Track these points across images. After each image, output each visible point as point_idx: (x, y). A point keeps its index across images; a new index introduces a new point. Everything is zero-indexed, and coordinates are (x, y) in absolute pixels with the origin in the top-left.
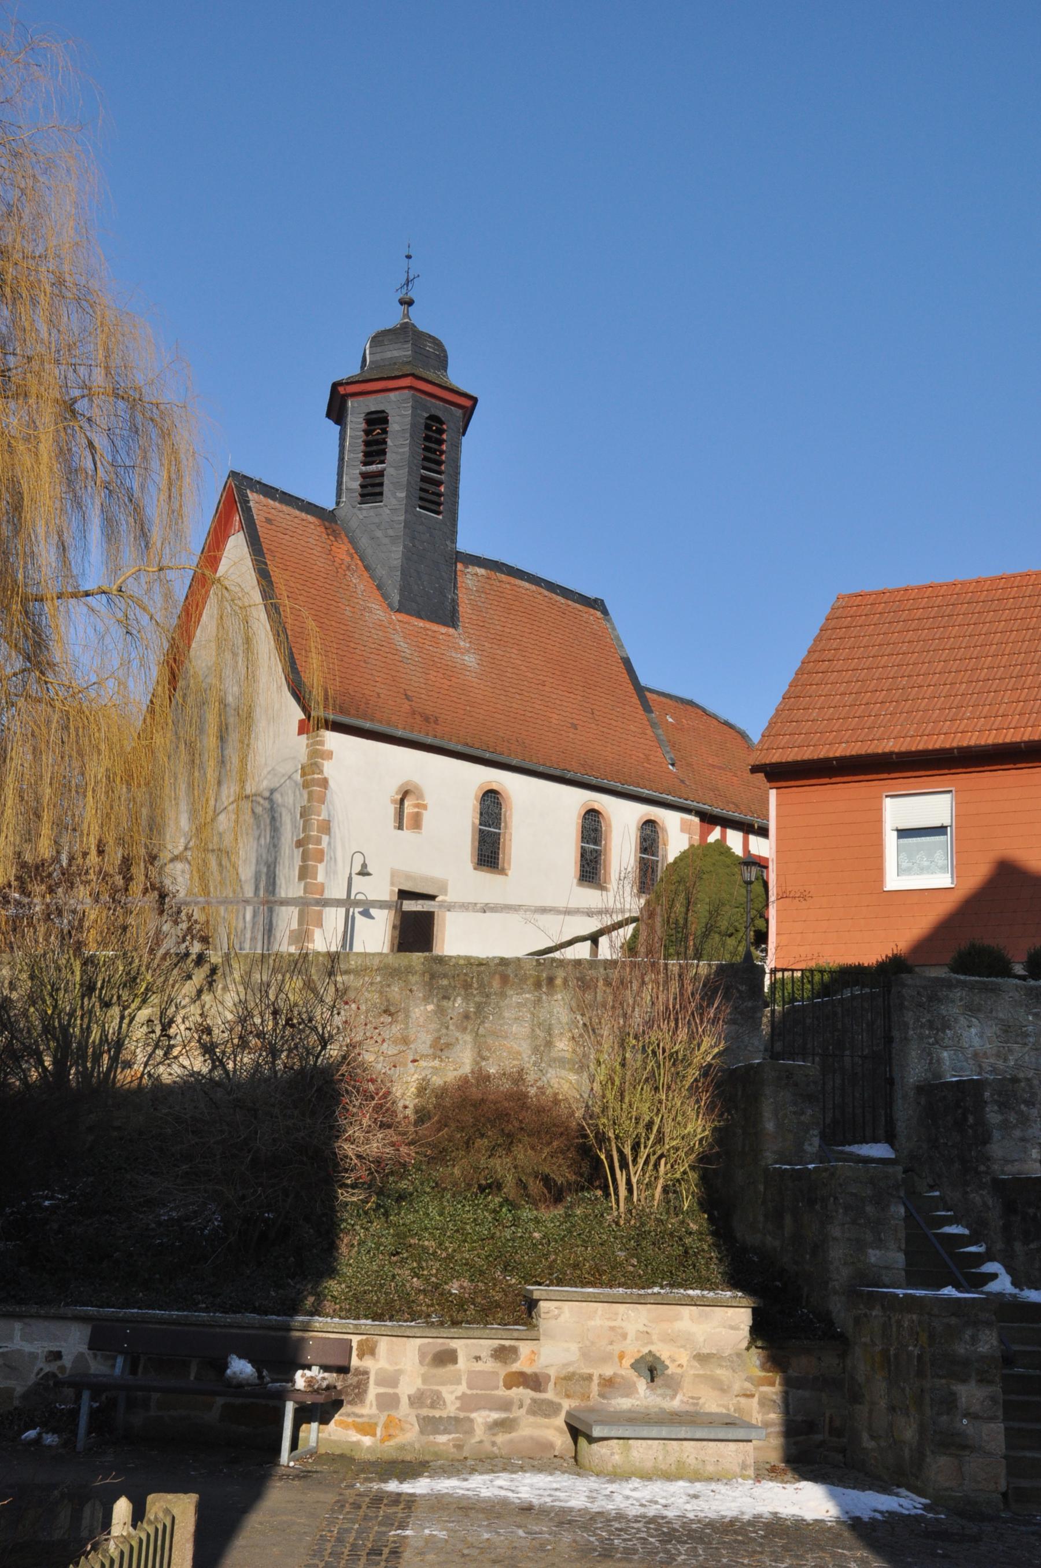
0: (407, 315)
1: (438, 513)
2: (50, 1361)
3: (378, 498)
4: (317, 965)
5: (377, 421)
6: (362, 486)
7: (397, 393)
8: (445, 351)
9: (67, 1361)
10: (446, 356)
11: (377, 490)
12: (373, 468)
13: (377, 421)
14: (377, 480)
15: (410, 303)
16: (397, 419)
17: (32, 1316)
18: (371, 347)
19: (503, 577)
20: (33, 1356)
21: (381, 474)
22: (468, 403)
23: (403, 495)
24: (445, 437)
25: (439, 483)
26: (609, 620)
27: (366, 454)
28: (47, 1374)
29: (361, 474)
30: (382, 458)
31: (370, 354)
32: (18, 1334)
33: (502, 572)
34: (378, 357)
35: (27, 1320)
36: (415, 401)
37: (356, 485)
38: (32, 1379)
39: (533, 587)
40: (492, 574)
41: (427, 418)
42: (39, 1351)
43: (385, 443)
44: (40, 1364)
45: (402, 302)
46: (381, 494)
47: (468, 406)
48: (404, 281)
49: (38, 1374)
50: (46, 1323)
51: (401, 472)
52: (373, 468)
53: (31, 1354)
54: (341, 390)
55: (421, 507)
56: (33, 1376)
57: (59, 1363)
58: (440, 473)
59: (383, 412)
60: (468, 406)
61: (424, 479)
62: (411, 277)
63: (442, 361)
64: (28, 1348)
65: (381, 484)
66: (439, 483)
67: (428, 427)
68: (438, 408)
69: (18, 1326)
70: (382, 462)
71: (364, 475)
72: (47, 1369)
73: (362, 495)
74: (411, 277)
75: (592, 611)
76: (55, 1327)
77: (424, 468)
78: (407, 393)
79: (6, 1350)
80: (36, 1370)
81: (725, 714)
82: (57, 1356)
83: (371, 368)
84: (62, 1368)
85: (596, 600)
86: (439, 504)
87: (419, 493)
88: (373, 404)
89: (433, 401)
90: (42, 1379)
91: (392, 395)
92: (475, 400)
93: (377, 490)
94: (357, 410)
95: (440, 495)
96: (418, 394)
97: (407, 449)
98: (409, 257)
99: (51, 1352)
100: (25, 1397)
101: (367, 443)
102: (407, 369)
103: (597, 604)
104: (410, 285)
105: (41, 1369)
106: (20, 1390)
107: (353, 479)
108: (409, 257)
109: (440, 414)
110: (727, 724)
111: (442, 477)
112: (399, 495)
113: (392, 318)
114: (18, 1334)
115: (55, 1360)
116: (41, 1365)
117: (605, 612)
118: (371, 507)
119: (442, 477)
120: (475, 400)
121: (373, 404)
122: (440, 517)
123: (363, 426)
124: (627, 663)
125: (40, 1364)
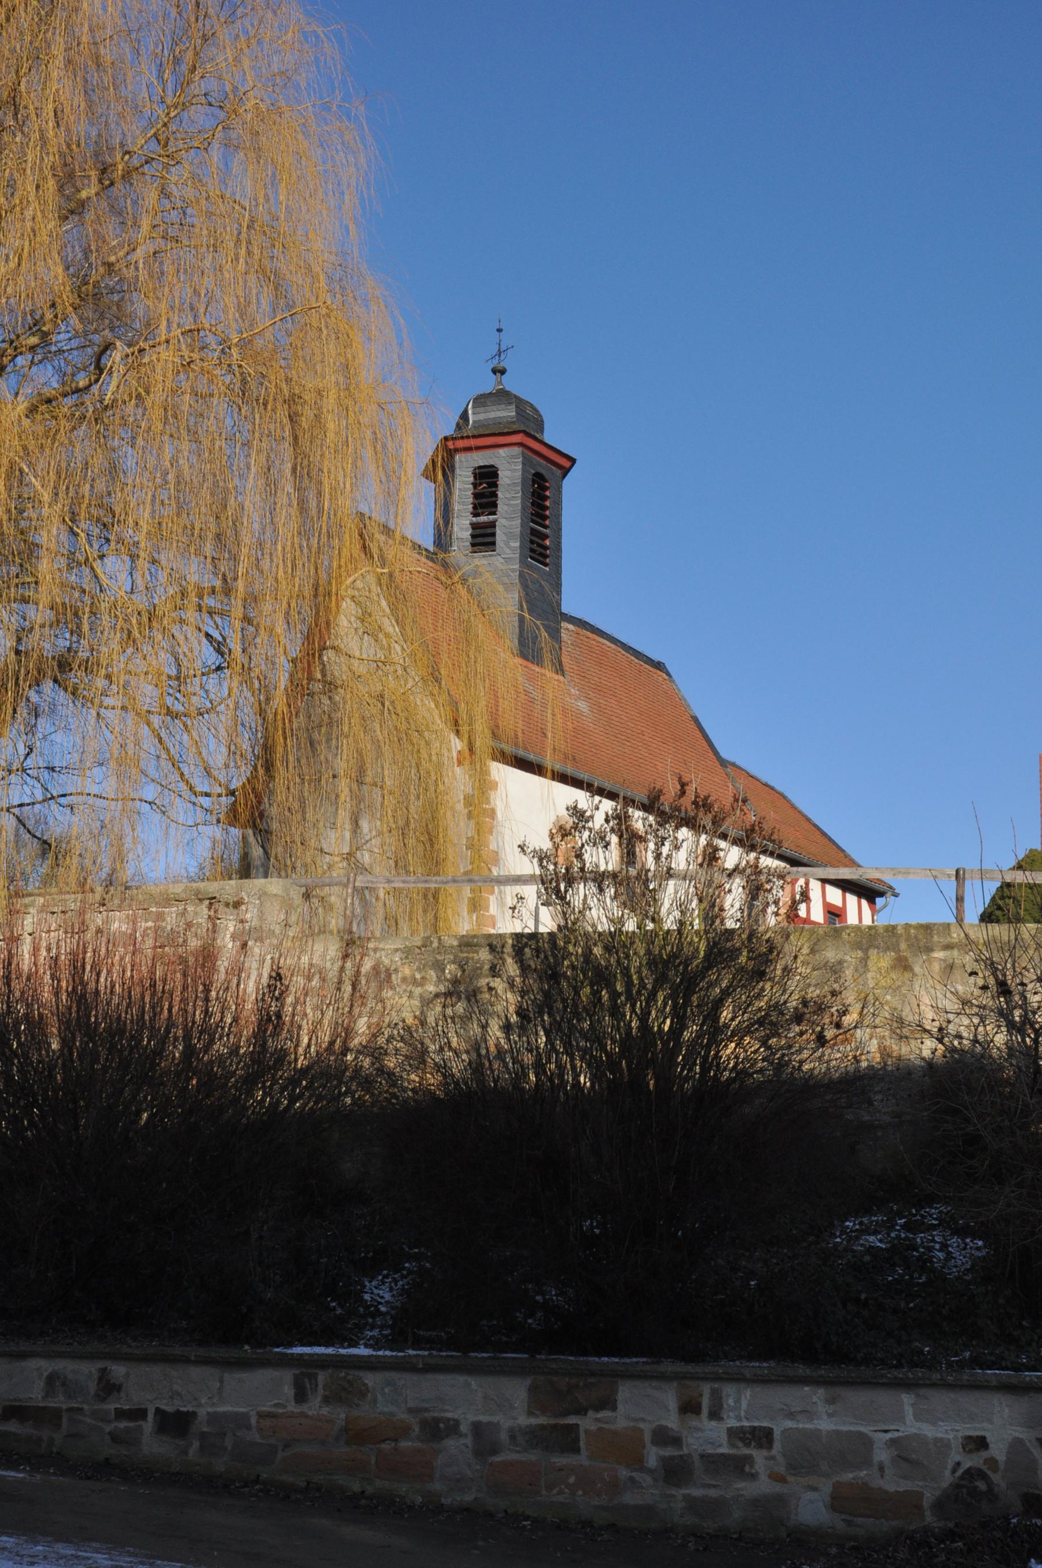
0: (500, 383)
1: (546, 565)
2: (970, 1451)
3: (491, 547)
4: (907, 940)
5: (486, 477)
6: (473, 536)
7: (506, 449)
8: (540, 416)
9: (998, 1451)
10: (542, 421)
11: (489, 539)
12: (483, 519)
13: (486, 477)
14: (489, 531)
15: (503, 372)
16: (508, 473)
17: (933, 1385)
18: (473, 407)
19: (589, 634)
20: (942, 1445)
21: (493, 525)
22: (567, 464)
23: (518, 544)
24: (548, 493)
25: (545, 537)
26: (673, 681)
27: (475, 508)
28: (968, 1472)
29: (471, 524)
30: (493, 510)
31: (474, 414)
32: (909, 1411)
33: (587, 630)
34: (482, 417)
35: (922, 1391)
36: (523, 454)
37: (467, 534)
38: (947, 1479)
39: (613, 646)
40: (579, 630)
41: (534, 475)
42: (951, 1437)
43: (496, 496)
44: (955, 1455)
45: (495, 371)
46: (494, 543)
47: (565, 464)
48: (495, 351)
49: (954, 1471)
50: (952, 1395)
51: (513, 523)
52: (483, 519)
53: (936, 1440)
54: (450, 445)
55: (532, 558)
56: (947, 1473)
57: (985, 1454)
58: (546, 527)
59: (492, 466)
60: (565, 464)
61: (533, 532)
62: (503, 348)
63: (540, 424)
64: (929, 1431)
65: (494, 535)
66: (545, 537)
67: (534, 482)
68: (544, 467)
69: (907, 1399)
70: (494, 513)
71: (474, 526)
72: (967, 1464)
73: (473, 545)
74: (503, 348)
75: (660, 673)
76: (968, 1400)
77: (533, 521)
78: (517, 450)
79: (896, 1435)
80: (950, 1466)
81: (765, 779)
82: (981, 1443)
83: (474, 427)
84: (992, 1462)
85: (659, 663)
86: (546, 556)
87: (528, 545)
88: (481, 459)
89: (538, 459)
90: (962, 1478)
91: (502, 452)
92: (573, 461)
93: (489, 539)
94: (465, 466)
95: (546, 548)
96: (526, 451)
97: (519, 501)
98: (499, 330)
99: (970, 1437)
100: (939, 1505)
101: (476, 496)
102: (516, 427)
103: (659, 666)
104: (503, 356)
105: (958, 1464)
106: (929, 1497)
107: (462, 529)
108: (499, 330)
109: (543, 472)
110: (766, 785)
111: (547, 531)
112: (512, 544)
113: (489, 384)
114: (909, 1411)
115: (978, 1450)
116: (958, 1458)
117: (668, 674)
118: (484, 556)
119: (547, 531)
120: (573, 461)
121: (481, 459)
122: (547, 569)
123: (472, 479)
124: (696, 720)
125: (955, 1455)
